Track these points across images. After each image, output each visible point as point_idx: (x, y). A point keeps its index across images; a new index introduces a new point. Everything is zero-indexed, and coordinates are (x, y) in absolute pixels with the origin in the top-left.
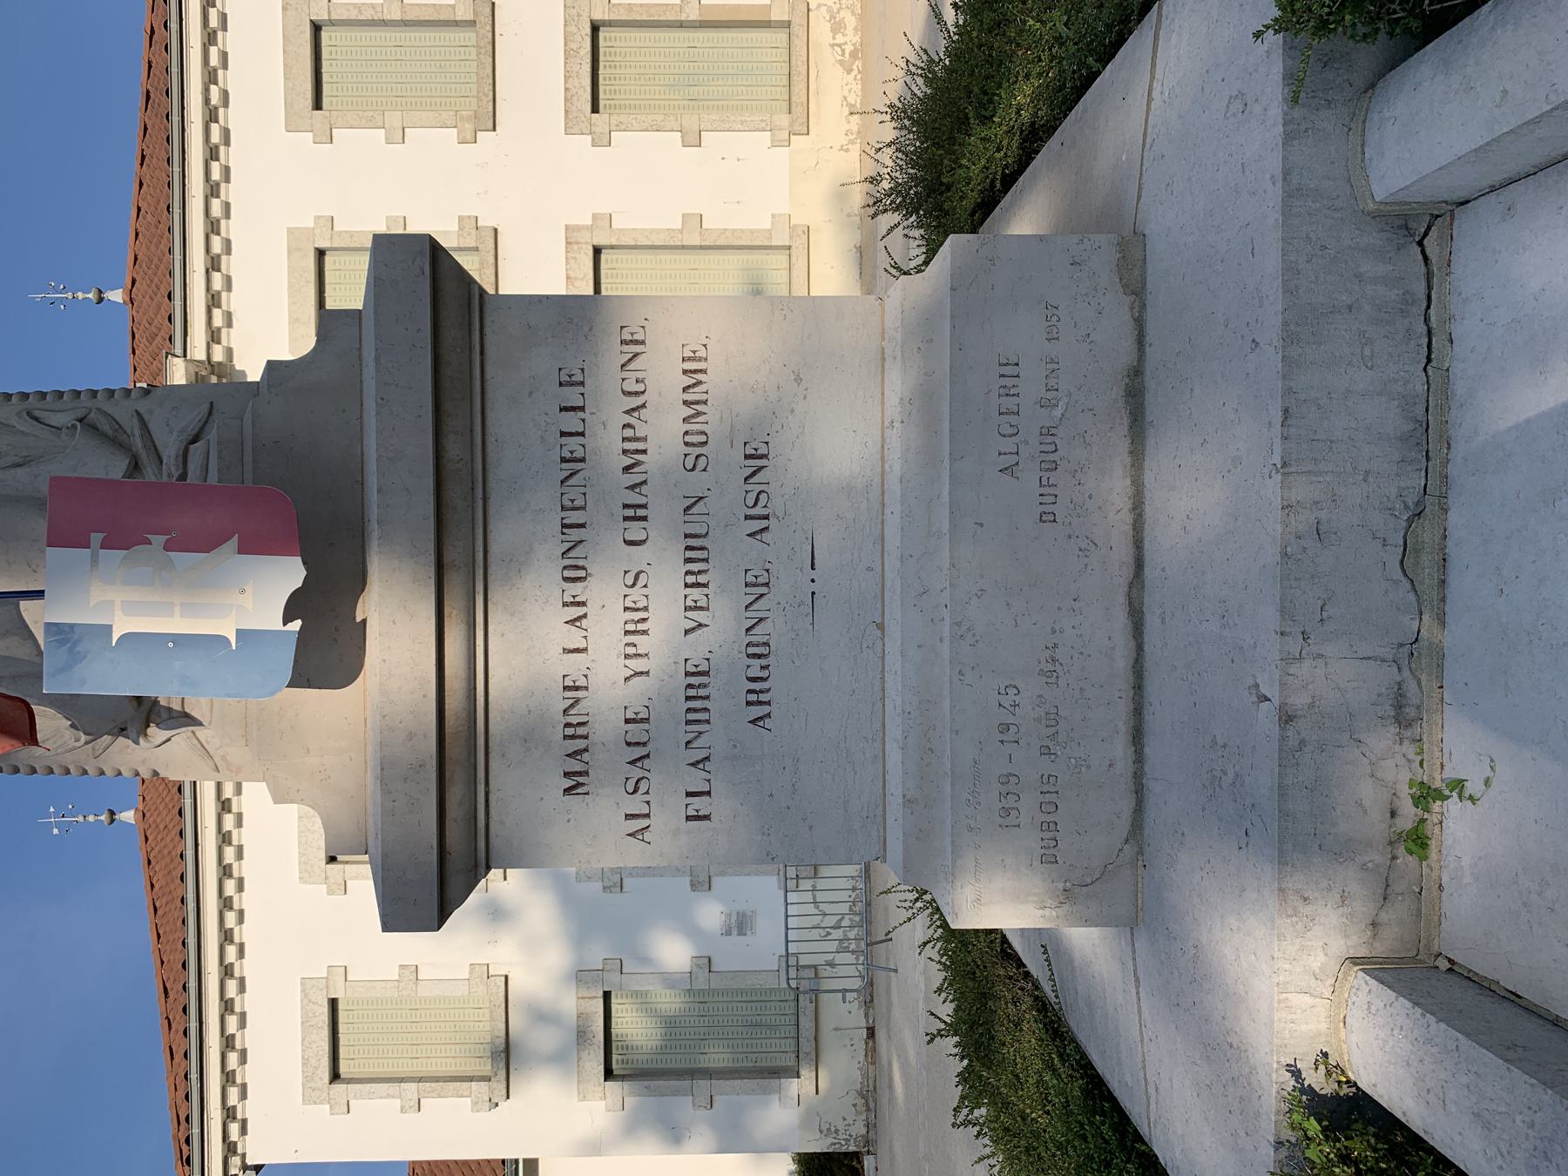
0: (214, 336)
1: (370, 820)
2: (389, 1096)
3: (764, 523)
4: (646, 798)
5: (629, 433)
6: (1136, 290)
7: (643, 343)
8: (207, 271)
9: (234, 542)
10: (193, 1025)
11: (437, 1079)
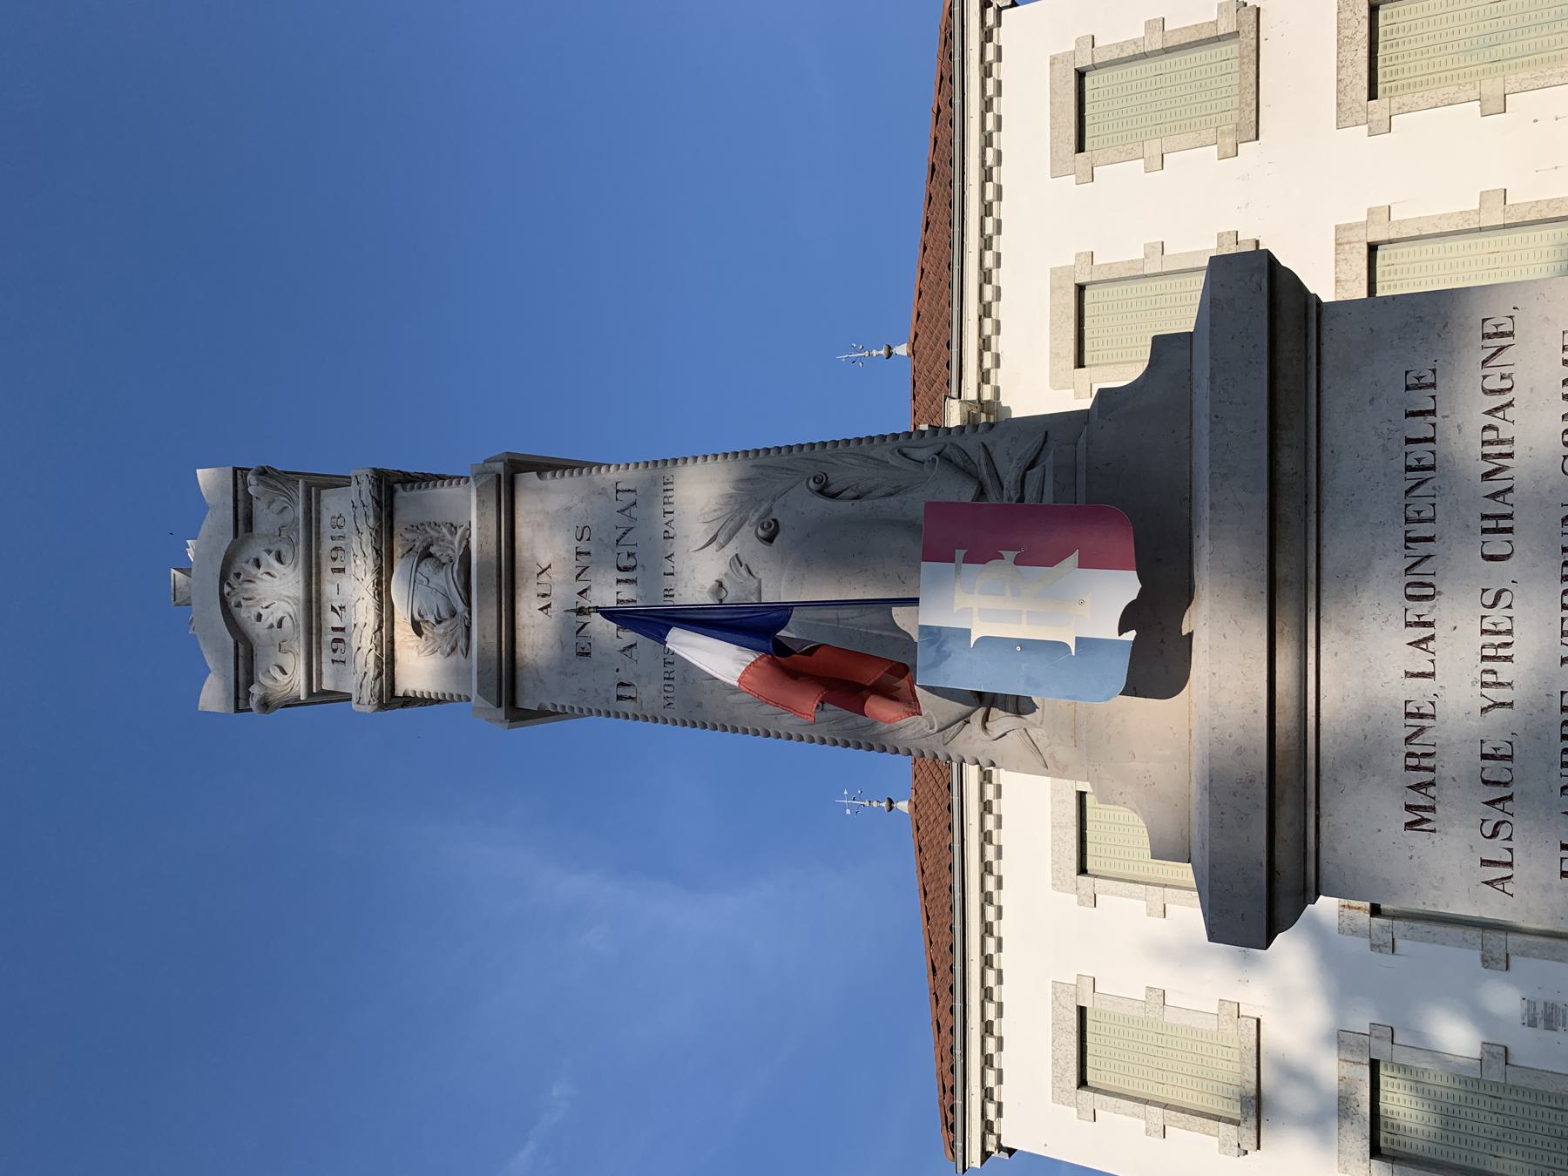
0: (984, 377)
1: (1195, 832)
2: (1133, 1115)
4: (1508, 844)
7: (1511, 334)
10: (958, 1005)
11: (1183, 1110)
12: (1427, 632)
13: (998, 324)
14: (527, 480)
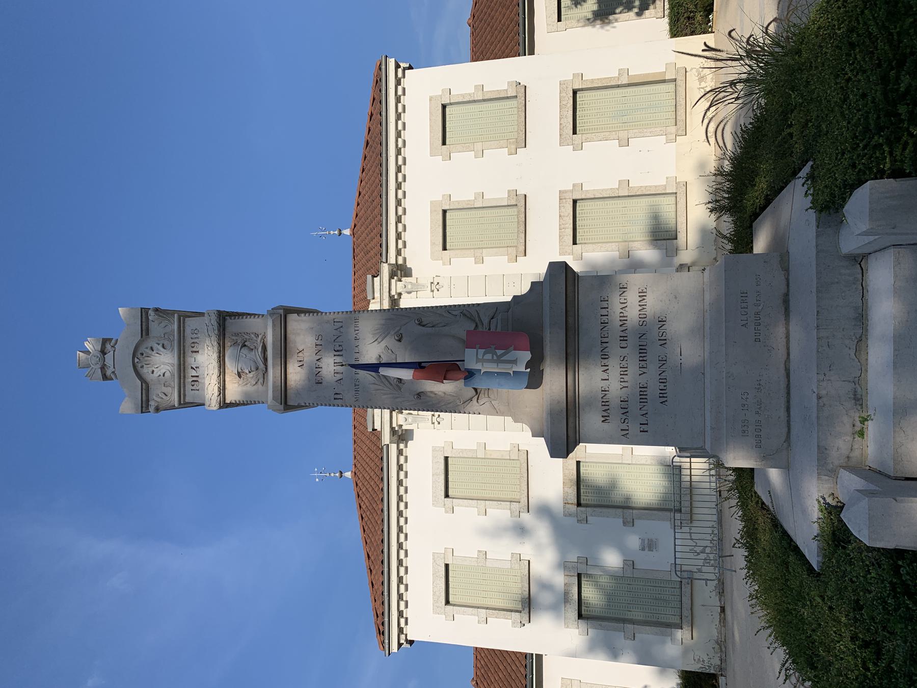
0: (399, 252)
2: (472, 614)
6: (787, 270)
9: (512, 348)
10: (386, 570)
13: (405, 226)
14: (292, 317)
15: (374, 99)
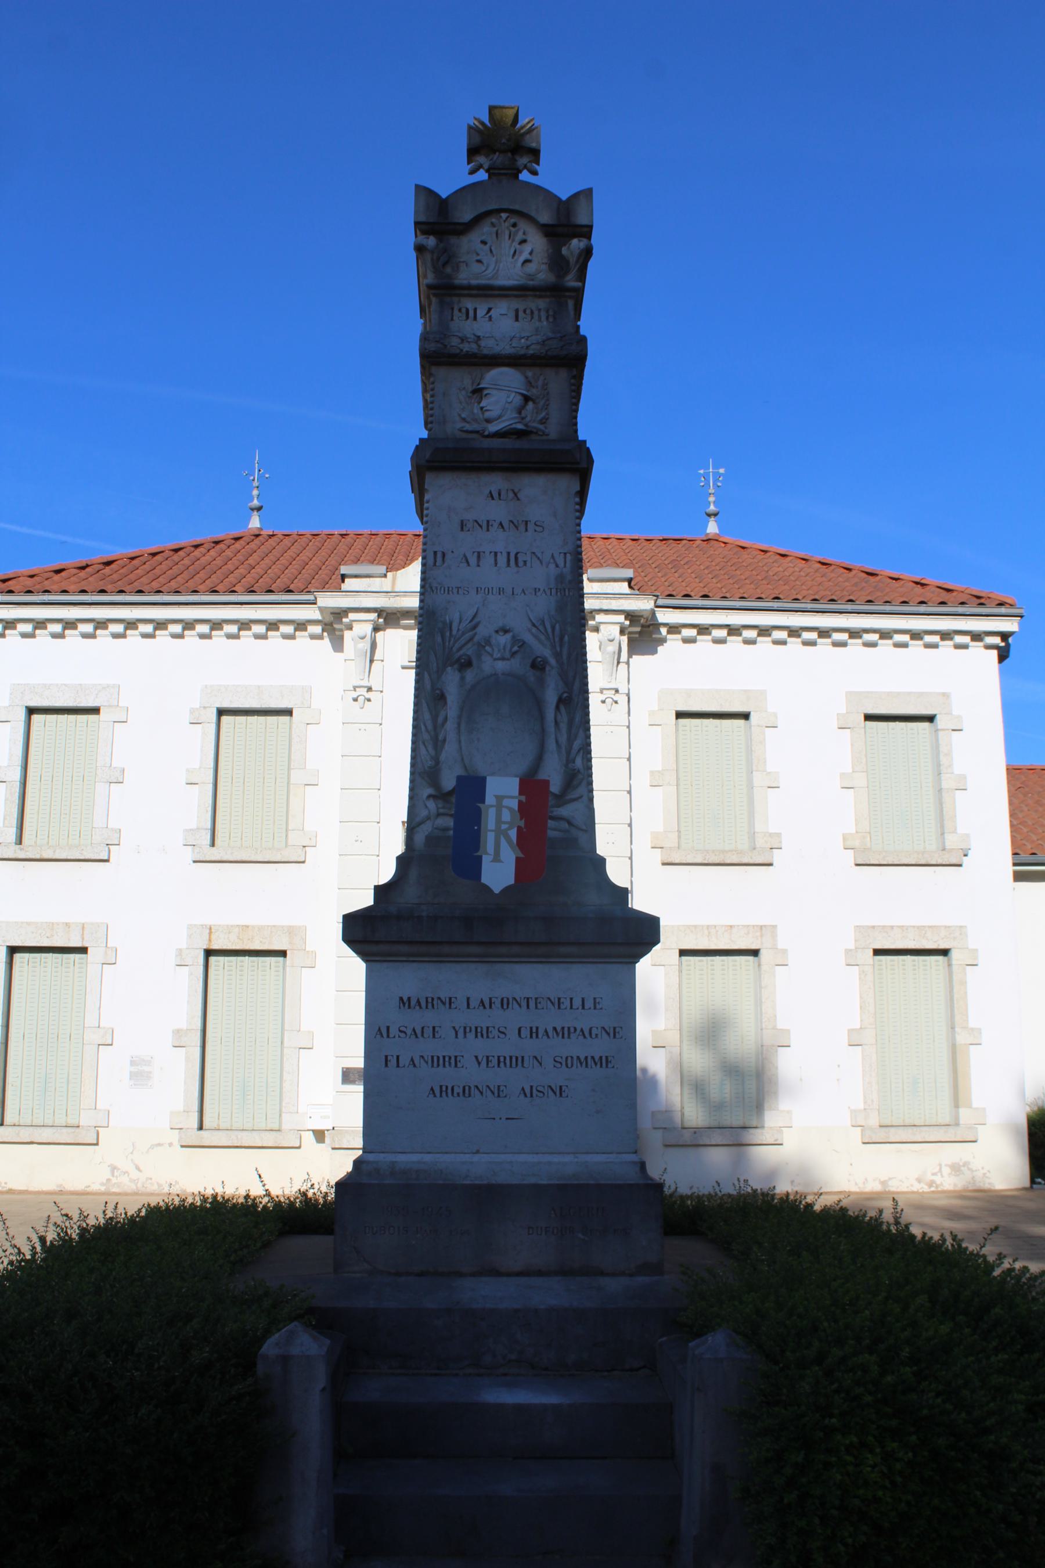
0: (674, 629)
3: (528, 1095)
5: (572, 1030)
8: (728, 626)
9: (521, 855)
12: (487, 1006)
15: (948, 590)
